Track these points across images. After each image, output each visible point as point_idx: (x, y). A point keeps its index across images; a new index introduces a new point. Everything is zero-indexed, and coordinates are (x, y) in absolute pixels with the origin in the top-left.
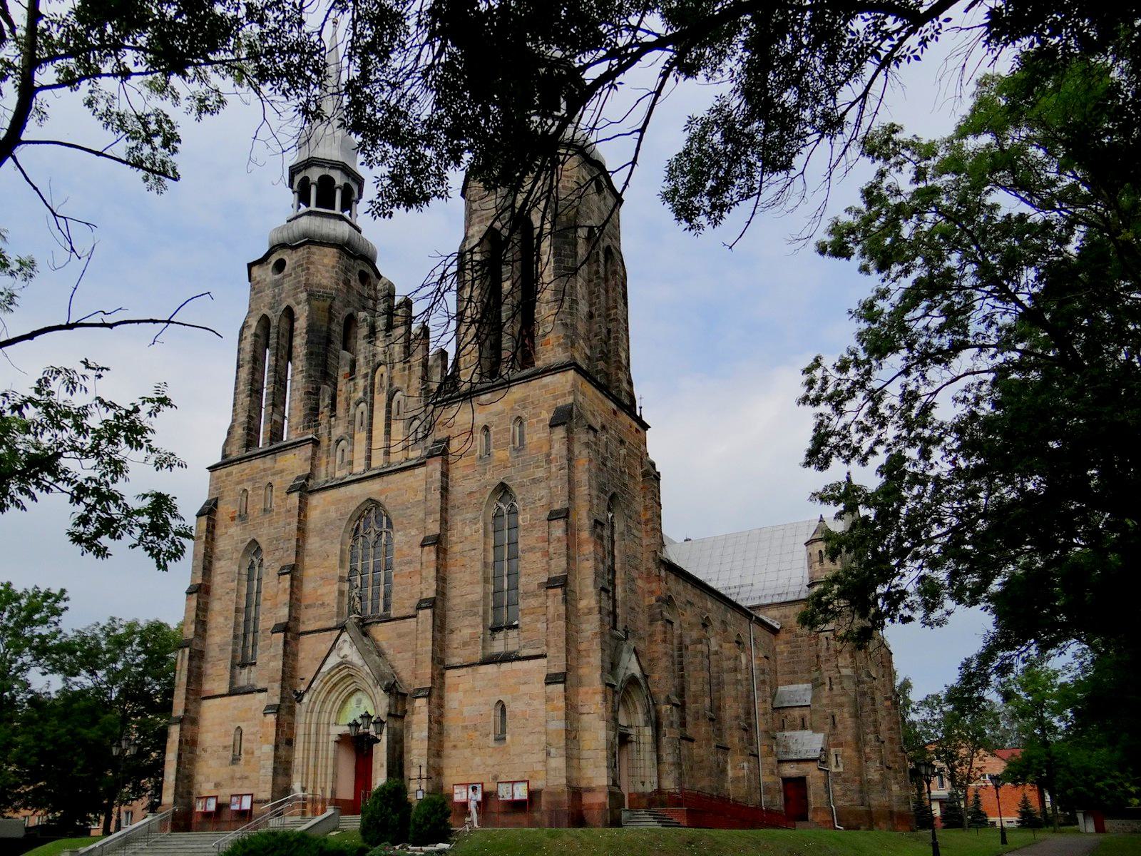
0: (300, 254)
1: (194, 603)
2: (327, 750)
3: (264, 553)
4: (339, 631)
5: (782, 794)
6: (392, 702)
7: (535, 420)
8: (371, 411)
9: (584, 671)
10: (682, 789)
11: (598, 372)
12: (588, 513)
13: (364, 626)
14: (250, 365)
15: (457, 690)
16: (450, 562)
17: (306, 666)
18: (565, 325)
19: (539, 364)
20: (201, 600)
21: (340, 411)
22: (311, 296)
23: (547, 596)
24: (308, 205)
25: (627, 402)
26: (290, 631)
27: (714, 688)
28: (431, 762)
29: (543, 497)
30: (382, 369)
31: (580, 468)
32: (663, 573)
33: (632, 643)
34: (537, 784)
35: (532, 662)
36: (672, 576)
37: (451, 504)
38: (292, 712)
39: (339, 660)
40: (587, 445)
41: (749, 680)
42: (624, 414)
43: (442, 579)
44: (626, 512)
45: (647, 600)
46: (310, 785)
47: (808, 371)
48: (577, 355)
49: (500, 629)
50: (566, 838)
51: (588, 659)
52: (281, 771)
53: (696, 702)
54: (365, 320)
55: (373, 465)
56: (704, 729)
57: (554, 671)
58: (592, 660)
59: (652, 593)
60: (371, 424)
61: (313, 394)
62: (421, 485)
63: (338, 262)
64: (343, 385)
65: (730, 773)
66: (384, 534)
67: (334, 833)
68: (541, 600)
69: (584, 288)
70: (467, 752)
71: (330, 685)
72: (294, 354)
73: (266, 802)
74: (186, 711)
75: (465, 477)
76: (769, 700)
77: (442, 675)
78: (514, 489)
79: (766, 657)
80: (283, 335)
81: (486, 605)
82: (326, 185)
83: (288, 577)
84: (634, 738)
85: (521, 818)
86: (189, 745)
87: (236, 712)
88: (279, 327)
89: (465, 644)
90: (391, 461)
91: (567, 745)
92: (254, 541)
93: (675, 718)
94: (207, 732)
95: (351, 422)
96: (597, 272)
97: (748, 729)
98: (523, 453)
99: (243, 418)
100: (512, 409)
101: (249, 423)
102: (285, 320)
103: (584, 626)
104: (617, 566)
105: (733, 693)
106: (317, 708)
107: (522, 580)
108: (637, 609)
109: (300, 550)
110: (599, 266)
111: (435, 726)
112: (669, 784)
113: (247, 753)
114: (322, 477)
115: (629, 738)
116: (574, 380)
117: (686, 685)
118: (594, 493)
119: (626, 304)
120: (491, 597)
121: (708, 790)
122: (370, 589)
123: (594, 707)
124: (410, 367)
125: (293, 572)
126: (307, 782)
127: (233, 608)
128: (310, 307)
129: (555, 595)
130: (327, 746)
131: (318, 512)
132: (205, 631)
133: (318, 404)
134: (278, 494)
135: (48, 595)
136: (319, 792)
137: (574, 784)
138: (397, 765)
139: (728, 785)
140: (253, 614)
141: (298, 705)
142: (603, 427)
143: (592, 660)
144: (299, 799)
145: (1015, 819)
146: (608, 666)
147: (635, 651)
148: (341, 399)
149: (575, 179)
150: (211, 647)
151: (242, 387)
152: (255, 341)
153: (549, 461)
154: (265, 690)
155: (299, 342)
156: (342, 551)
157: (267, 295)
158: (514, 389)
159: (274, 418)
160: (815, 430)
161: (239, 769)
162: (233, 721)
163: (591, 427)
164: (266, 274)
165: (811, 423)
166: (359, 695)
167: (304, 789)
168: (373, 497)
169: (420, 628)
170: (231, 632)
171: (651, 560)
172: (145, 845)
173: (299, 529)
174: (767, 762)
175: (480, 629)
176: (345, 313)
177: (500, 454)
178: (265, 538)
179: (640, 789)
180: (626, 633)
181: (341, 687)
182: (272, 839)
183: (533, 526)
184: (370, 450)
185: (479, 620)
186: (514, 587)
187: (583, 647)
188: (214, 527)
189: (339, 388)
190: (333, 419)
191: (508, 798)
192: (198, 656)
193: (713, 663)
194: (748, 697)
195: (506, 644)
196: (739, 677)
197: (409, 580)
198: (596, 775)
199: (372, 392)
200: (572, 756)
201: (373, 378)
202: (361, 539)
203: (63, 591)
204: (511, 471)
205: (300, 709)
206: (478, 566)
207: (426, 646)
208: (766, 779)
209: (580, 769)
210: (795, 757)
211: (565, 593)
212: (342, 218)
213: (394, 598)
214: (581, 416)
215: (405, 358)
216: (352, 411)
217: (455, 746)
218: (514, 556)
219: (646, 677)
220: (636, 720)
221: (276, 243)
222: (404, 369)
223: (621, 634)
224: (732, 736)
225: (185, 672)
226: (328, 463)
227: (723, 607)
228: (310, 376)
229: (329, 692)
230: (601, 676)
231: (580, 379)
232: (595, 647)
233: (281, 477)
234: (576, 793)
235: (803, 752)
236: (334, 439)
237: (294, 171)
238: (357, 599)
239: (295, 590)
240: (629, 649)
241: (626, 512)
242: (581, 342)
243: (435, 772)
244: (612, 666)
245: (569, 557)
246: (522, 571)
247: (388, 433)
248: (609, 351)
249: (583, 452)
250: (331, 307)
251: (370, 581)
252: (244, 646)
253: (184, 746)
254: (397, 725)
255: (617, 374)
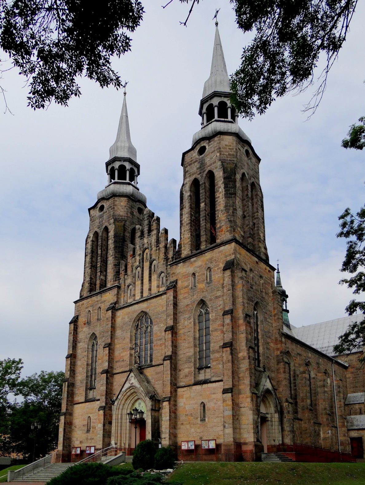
0: (110, 202)
1: (69, 362)
2: (126, 426)
3: (98, 339)
4: (129, 373)
5: (350, 446)
6: (153, 404)
7: (216, 268)
8: (143, 271)
9: (241, 387)
10: (294, 443)
11: (248, 244)
12: (242, 311)
13: (141, 370)
14: (91, 255)
15: (183, 398)
16: (179, 338)
17: (116, 388)
18: (230, 221)
19: (218, 241)
20: (72, 361)
21: (129, 272)
22: (116, 220)
23: (223, 352)
24: (114, 179)
25: (264, 257)
26: (109, 373)
27: (313, 395)
28: (171, 431)
29: (221, 305)
30: (147, 251)
31: (238, 289)
32: (283, 339)
33: (267, 373)
34: (220, 441)
35: (217, 383)
36: (290, 342)
37: (178, 311)
38: (111, 409)
39: (130, 385)
40: (242, 278)
41: (332, 391)
42: (262, 264)
43: (175, 346)
44: (264, 310)
45: (275, 353)
46: (119, 442)
47: (342, 217)
48: (236, 235)
49: (202, 369)
50: (229, 466)
51: (243, 381)
52: (106, 436)
53: (303, 401)
54: (139, 229)
55: (144, 296)
56: (307, 415)
57: (227, 387)
58: (245, 382)
59: (278, 349)
60: (142, 277)
61: (117, 265)
62: (165, 303)
63: (127, 204)
64: (130, 260)
65: (322, 435)
66: (149, 327)
67: (122, 464)
68: (221, 354)
69: (240, 203)
70: (188, 426)
71: (126, 397)
72: (109, 248)
73: (100, 449)
74: (67, 410)
75: (185, 298)
76: (343, 401)
77: (176, 391)
78: (207, 302)
79: (340, 380)
80: (104, 240)
81: (195, 358)
82: (122, 169)
83: (108, 348)
84: (269, 419)
85: (213, 457)
86: (69, 425)
87: (88, 410)
88: (102, 236)
89: (186, 376)
90: (152, 293)
91: (233, 422)
92: (94, 333)
93: (291, 409)
94: (76, 419)
95: (134, 277)
96: (247, 195)
97: (332, 414)
98: (211, 284)
99: (88, 279)
100: (206, 264)
101: (91, 281)
102: (105, 233)
103: (241, 366)
104: (260, 337)
105: (323, 397)
106: (121, 407)
107: (212, 345)
108: (270, 357)
109: (112, 336)
110: (248, 192)
111: (173, 415)
112: (288, 441)
113: (93, 428)
114: (122, 303)
115: (267, 419)
116: (235, 247)
117: (298, 393)
118: (245, 301)
119: (263, 210)
120: (198, 354)
121: (309, 444)
122: (144, 353)
123: (246, 404)
124: (159, 249)
125: (110, 346)
126: (117, 440)
127: (86, 363)
128: (115, 226)
129: (227, 351)
130: (126, 425)
131: (120, 318)
132: (74, 374)
133: (119, 270)
134: (103, 312)
135: (14, 362)
136: (123, 445)
137: (237, 441)
138: (157, 433)
139: (321, 441)
140: (94, 366)
141: (113, 406)
142: (251, 270)
143: (245, 382)
144: (114, 448)
145: (298, 442)
146: (254, 384)
147: (268, 377)
148: (129, 266)
149: (234, 150)
150: (77, 381)
151: (87, 265)
152: (92, 243)
153: (223, 287)
154: (99, 400)
155: (111, 242)
156: (131, 336)
157: (97, 222)
158: (206, 254)
159: (101, 277)
160: (348, 251)
161: (90, 435)
162: (87, 414)
163: (243, 270)
164: (96, 213)
165: (346, 247)
166: (139, 401)
167: (116, 444)
168: (144, 310)
169: (165, 369)
170: (85, 374)
171: (277, 334)
172: (42, 469)
173: (112, 327)
174: (341, 431)
175: (193, 369)
176: (131, 227)
177: (201, 286)
178: (98, 332)
179: (273, 443)
180: (264, 369)
181: (131, 397)
182: (85, 467)
183: (216, 319)
184: (142, 289)
185: (192, 364)
186: (208, 349)
187: (241, 375)
188: (77, 328)
189: (128, 261)
190: (126, 276)
191: (206, 447)
192: (72, 385)
193: (312, 383)
194: (331, 399)
195: (205, 376)
196: (326, 389)
197: (160, 348)
198: (249, 437)
199: (143, 262)
200: (236, 428)
201: (143, 256)
202: (139, 330)
203: (20, 360)
204: (205, 294)
205: (114, 407)
206: (191, 339)
207: (168, 378)
208: (341, 438)
209: (240, 434)
210: (356, 428)
211: (231, 350)
212: (129, 184)
213: (154, 356)
214: (238, 264)
215: (157, 245)
216: (134, 271)
217: (182, 424)
218: (208, 334)
219: (275, 390)
220: (269, 410)
221: (100, 198)
222: (157, 250)
223: (262, 369)
224: (322, 418)
225: (66, 393)
226: (124, 296)
227: (317, 356)
228: (116, 257)
229: (126, 400)
230: (250, 389)
231: (238, 247)
232: (247, 375)
233: (104, 304)
234: (238, 445)
235: (361, 425)
236: (127, 285)
237: (108, 164)
238: (137, 357)
239: (111, 354)
240: (266, 376)
241: (264, 310)
242: (239, 229)
243: (173, 435)
244: (256, 385)
245: (233, 333)
246: (212, 341)
247: (150, 280)
248: (254, 234)
249: (240, 282)
250: (124, 225)
251: (144, 349)
252: (91, 381)
253: (66, 425)
254: (156, 414)
255: (258, 244)
